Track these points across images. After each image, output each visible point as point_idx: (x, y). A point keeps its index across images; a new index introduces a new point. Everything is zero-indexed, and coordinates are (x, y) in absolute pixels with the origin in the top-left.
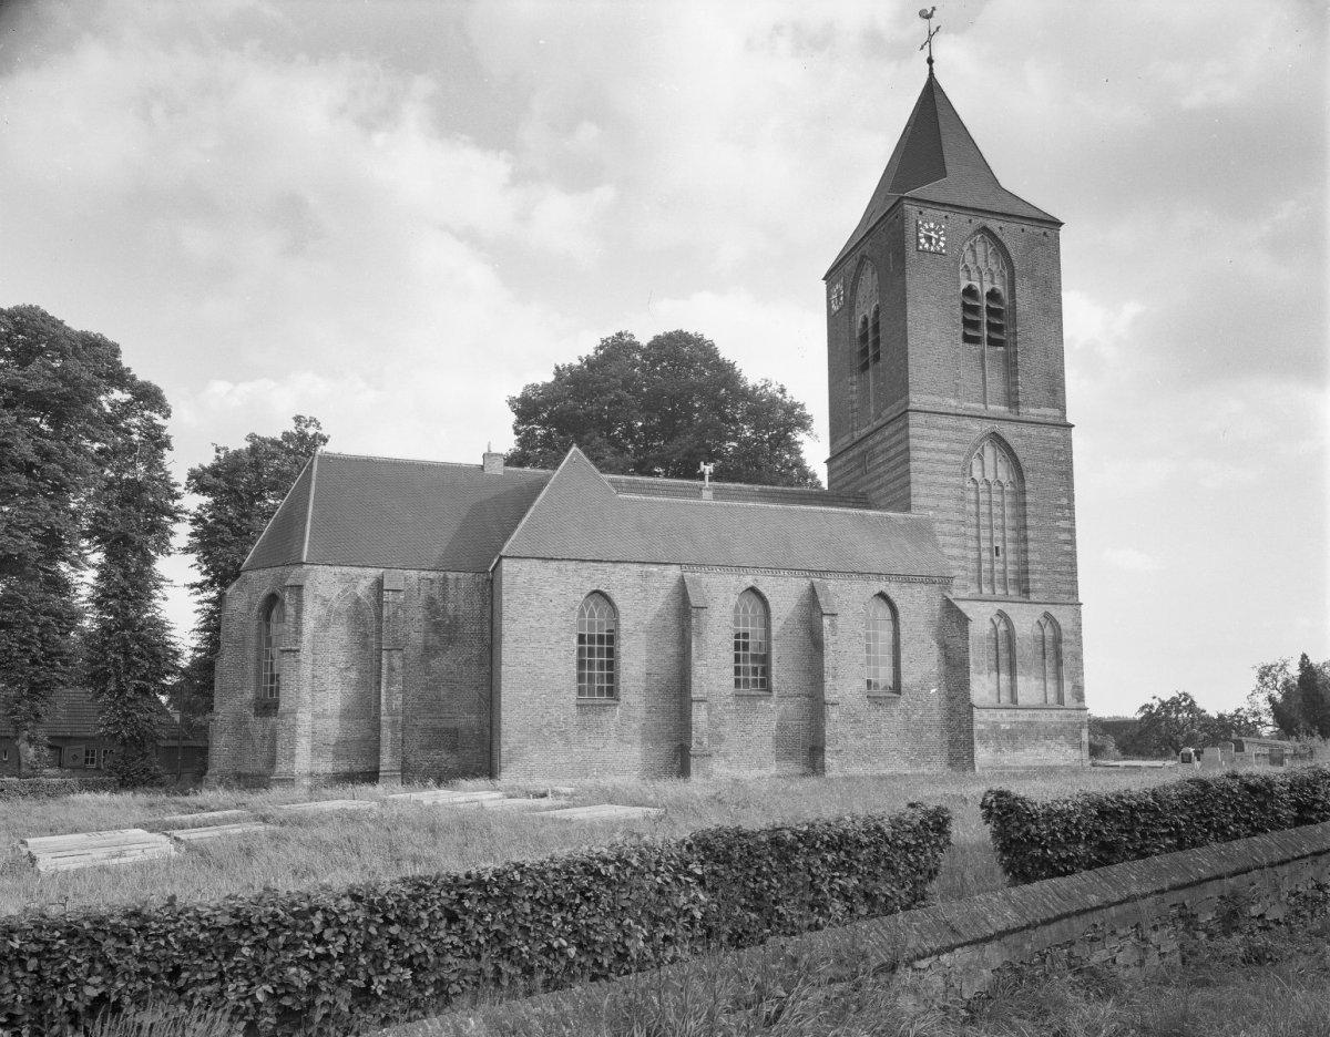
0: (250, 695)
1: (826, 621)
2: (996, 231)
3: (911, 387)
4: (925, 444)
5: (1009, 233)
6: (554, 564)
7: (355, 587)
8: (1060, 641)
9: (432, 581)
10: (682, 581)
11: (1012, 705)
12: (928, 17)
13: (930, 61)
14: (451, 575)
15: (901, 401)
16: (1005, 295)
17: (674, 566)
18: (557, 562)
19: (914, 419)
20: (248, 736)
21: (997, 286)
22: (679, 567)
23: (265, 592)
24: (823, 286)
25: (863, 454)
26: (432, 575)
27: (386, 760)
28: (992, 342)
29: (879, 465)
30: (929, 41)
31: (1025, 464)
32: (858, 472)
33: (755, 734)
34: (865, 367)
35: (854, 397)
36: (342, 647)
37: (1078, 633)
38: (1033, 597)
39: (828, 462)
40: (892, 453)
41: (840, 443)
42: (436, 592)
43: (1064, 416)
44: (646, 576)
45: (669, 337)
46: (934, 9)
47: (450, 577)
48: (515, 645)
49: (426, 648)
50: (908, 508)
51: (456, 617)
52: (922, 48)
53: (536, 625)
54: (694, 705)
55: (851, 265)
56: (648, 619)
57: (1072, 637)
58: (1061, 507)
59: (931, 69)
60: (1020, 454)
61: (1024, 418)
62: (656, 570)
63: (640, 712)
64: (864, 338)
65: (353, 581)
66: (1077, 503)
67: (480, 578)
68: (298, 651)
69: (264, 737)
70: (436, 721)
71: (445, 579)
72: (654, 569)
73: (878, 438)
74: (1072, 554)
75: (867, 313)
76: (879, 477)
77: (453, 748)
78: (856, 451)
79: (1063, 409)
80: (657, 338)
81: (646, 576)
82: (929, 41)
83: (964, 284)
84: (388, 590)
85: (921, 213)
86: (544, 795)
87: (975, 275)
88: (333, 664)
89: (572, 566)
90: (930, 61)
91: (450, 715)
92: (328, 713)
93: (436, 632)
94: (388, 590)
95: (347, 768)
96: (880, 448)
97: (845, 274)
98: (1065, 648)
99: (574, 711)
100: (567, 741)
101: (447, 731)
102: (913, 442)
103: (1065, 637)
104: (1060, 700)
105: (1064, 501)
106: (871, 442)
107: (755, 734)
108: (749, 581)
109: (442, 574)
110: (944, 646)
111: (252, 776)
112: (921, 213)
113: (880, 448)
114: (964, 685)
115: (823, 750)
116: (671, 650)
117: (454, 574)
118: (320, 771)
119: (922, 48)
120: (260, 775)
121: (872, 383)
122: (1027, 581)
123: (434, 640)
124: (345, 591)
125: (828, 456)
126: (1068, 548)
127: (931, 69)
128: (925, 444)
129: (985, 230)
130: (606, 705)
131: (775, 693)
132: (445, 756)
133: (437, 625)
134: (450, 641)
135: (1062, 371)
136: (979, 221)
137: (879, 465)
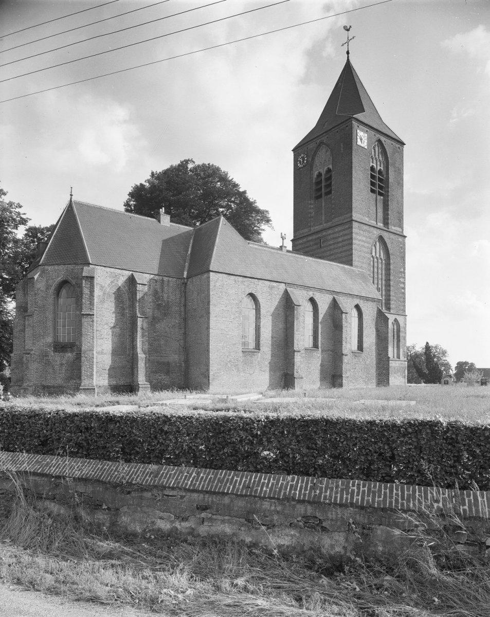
0: (50, 339)
1: (344, 316)
2: (383, 142)
3: (353, 210)
4: (358, 237)
5: (386, 142)
6: (233, 277)
7: (117, 281)
8: (399, 331)
9: (156, 281)
10: (286, 292)
11: (398, 359)
12: (348, 30)
13: (348, 53)
14: (165, 279)
15: (348, 215)
16: (384, 173)
17: (283, 284)
18: (234, 277)
19: (355, 225)
20: (48, 363)
21: (382, 168)
22: (284, 284)
23: (60, 279)
24: (291, 156)
25: (320, 238)
26: (156, 278)
27: (141, 378)
28: (380, 194)
29: (330, 245)
30: (348, 43)
31: (391, 252)
32: (315, 247)
33: (312, 368)
34: (319, 197)
35: (312, 211)
36: (114, 312)
37: (405, 328)
38: (392, 311)
39: (292, 241)
40: (340, 239)
41: (301, 232)
42: (158, 287)
43: (402, 232)
44: (271, 288)
45: (210, 167)
46: (350, 27)
47: (165, 280)
48: (216, 319)
49: (154, 318)
50: (351, 265)
51: (168, 301)
52: (343, 45)
53: (225, 309)
54: (296, 354)
55: (312, 146)
56: (272, 309)
57: (403, 330)
58: (401, 272)
59: (348, 57)
60: (389, 246)
61: (391, 231)
62: (275, 285)
63: (268, 357)
64: (319, 183)
65: (116, 277)
66: (406, 271)
67: (179, 282)
68: (93, 315)
69: (62, 364)
70: (159, 358)
71: (163, 280)
72: (275, 284)
73: (330, 232)
74: (404, 294)
75: (321, 171)
76: (330, 250)
77: (168, 373)
78: (314, 237)
79: (402, 227)
80: (204, 165)
81: (271, 288)
82: (348, 43)
83: (371, 164)
84: (139, 284)
85: (358, 127)
86: (148, 406)
87: (375, 161)
88: (107, 324)
89: (241, 279)
90: (348, 53)
91: (165, 355)
92: (105, 351)
93: (158, 309)
94: (139, 284)
95: (115, 383)
96: (332, 236)
97: (305, 152)
98: (401, 334)
99: (241, 354)
100: (238, 370)
101: (164, 363)
102: (354, 235)
103: (401, 329)
104: (398, 357)
105: (402, 270)
106: (324, 233)
107: (312, 368)
108: (311, 294)
109: (161, 278)
110: (377, 330)
111: (54, 387)
112: (358, 127)
113: (332, 236)
114: (386, 349)
115: (341, 376)
116: (281, 326)
117: (166, 278)
118: (101, 385)
119: (343, 45)
120: (60, 387)
121: (323, 205)
122: (390, 304)
123: (158, 314)
124: (112, 282)
125: (292, 238)
126: (403, 291)
127: (348, 57)
128: (358, 237)
129: (379, 141)
130: (254, 352)
131: (320, 349)
132: (164, 377)
133: (159, 305)
134: (165, 315)
135: (403, 211)
136: (378, 136)
137: (330, 245)
